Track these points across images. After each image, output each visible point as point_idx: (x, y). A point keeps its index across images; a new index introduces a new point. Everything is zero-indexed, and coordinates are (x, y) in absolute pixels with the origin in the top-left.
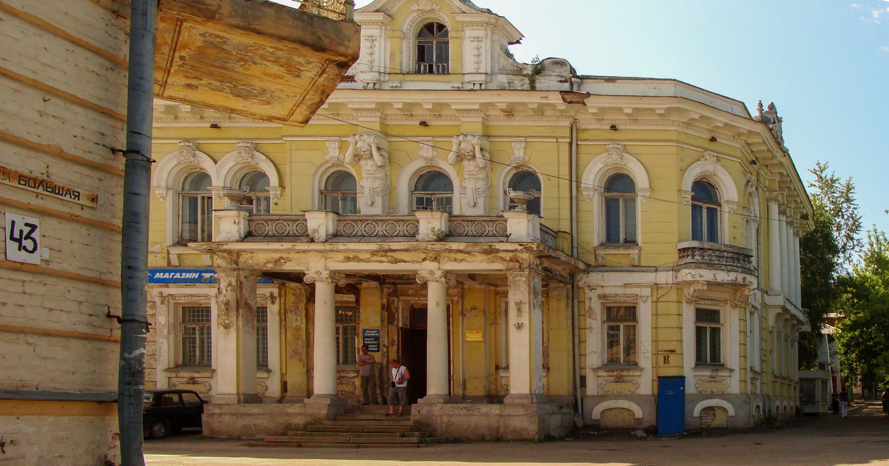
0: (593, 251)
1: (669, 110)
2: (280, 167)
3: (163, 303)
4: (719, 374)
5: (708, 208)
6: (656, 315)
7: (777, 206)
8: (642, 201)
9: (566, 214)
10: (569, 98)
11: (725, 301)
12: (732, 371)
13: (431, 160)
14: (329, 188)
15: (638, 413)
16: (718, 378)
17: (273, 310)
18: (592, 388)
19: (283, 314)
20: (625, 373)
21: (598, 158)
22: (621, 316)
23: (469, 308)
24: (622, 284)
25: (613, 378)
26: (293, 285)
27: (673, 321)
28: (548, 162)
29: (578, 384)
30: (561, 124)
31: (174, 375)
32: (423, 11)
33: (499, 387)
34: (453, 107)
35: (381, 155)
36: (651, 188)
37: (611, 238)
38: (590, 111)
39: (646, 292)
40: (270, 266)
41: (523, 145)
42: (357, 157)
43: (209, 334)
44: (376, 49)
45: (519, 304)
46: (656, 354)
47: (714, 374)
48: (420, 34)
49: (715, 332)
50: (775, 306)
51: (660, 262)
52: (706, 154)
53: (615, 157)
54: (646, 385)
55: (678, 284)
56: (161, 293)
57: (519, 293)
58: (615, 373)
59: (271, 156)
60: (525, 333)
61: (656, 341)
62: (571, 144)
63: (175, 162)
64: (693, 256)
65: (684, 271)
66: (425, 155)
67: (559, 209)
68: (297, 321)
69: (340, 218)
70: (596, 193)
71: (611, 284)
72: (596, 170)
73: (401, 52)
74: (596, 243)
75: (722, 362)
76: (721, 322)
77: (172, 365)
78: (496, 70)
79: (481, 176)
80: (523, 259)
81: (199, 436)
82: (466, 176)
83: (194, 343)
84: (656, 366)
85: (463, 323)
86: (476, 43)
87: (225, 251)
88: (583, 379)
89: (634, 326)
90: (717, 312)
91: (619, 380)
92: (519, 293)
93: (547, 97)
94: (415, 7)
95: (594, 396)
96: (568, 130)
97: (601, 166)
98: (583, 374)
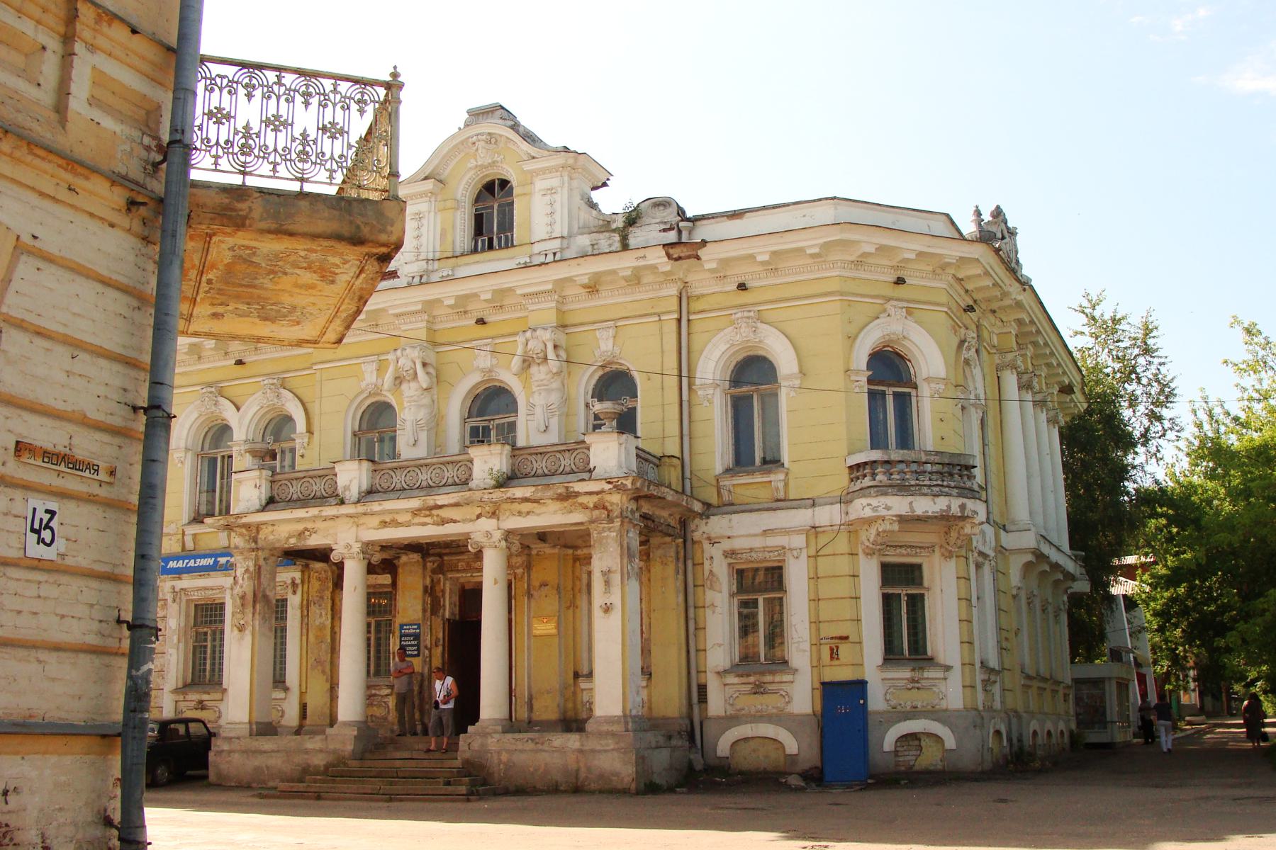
0: (714, 482)
1: (827, 246)
4: (926, 675)
5: (895, 395)
6: (815, 578)
7: (1015, 376)
8: (788, 394)
10: (675, 252)
11: (931, 548)
12: (948, 668)
13: (490, 371)
15: (791, 746)
16: (924, 683)
17: (294, 601)
18: (716, 704)
19: (306, 607)
20: (768, 678)
21: (718, 336)
22: (760, 583)
24: (759, 531)
26: (318, 566)
27: (843, 587)
30: (664, 292)
31: (181, 698)
32: (482, 167)
34: (519, 292)
36: (803, 373)
37: (742, 459)
38: (707, 266)
40: (293, 541)
42: (399, 380)
43: (222, 639)
45: (606, 574)
46: (816, 645)
47: (917, 675)
48: (477, 200)
49: (916, 602)
50: (1020, 551)
53: (745, 331)
54: (801, 696)
56: (173, 588)
58: (752, 679)
59: (299, 392)
61: (816, 623)
62: (679, 320)
63: (195, 415)
64: (874, 475)
67: (663, 421)
68: (321, 617)
72: (717, 354)
73: (454, 227)
74: (719, 469)
75: (929, 653)
76: (926, 583)
77: (180, 685)
80: (612, 504)
83: (205, 653)
84: (817, 666)
86: (548, 197)
88: (702, 689)
89: (781, 599)
90: (919, 567)
91: (759, 689)
92: (607, 557)
94: (472, 163)
95: (719, 718)
96: (675, 301)
97: (723, 347)
98: (703, 681)
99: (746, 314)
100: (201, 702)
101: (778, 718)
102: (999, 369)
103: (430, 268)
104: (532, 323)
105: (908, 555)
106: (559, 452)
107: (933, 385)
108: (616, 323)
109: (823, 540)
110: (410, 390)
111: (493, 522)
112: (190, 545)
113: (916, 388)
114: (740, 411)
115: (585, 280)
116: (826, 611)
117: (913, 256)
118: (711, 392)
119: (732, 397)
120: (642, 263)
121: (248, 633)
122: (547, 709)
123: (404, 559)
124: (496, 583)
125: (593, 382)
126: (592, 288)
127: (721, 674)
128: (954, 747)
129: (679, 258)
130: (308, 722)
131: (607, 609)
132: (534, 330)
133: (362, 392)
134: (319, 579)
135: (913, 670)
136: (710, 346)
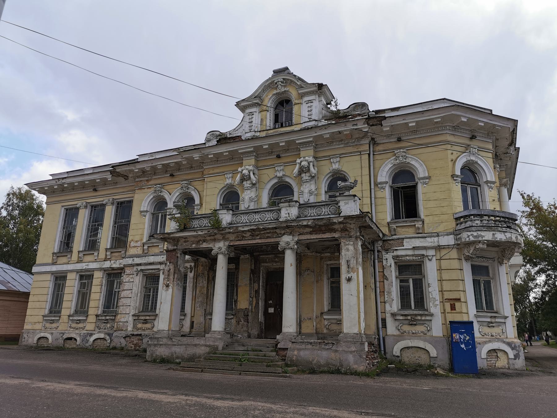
6: (440, 270)
10: (371, 122)
12: (506, 318)
15: (433, 353)
17: (191, 275)
18: (391, 328)
19: (196, 278)
22: (411, 270)
24: (411, 247)
26: (203, 259)
29: (380, 326)
42: (243, 179)
43: (157, 292)
46: (443, 301)
51: (441, 229)
54: (438, 328)
55: (458, 245)
62: (369, 154)
68: (203, 283)
69: (234, 213)
71: (409, 246)
72: (387, 168)
74: (389, 220)
83: (149, 298)
84: (444, 312)
87: (171, 238)
88: (384, 321)
90: (487, 268)
93: (356, 125)
96: (368, 145)
97: (390, 166)
100: (145, 320)
106: (322, 205)
111: (291, 237)
113: (480, 186)
121: (170, 290)
123: (242, 257)
124: (291, 265)
125: (328, 182)
128: (435, 356)
129: (373, 125)
131: (349, 280)
134: (202, 266)
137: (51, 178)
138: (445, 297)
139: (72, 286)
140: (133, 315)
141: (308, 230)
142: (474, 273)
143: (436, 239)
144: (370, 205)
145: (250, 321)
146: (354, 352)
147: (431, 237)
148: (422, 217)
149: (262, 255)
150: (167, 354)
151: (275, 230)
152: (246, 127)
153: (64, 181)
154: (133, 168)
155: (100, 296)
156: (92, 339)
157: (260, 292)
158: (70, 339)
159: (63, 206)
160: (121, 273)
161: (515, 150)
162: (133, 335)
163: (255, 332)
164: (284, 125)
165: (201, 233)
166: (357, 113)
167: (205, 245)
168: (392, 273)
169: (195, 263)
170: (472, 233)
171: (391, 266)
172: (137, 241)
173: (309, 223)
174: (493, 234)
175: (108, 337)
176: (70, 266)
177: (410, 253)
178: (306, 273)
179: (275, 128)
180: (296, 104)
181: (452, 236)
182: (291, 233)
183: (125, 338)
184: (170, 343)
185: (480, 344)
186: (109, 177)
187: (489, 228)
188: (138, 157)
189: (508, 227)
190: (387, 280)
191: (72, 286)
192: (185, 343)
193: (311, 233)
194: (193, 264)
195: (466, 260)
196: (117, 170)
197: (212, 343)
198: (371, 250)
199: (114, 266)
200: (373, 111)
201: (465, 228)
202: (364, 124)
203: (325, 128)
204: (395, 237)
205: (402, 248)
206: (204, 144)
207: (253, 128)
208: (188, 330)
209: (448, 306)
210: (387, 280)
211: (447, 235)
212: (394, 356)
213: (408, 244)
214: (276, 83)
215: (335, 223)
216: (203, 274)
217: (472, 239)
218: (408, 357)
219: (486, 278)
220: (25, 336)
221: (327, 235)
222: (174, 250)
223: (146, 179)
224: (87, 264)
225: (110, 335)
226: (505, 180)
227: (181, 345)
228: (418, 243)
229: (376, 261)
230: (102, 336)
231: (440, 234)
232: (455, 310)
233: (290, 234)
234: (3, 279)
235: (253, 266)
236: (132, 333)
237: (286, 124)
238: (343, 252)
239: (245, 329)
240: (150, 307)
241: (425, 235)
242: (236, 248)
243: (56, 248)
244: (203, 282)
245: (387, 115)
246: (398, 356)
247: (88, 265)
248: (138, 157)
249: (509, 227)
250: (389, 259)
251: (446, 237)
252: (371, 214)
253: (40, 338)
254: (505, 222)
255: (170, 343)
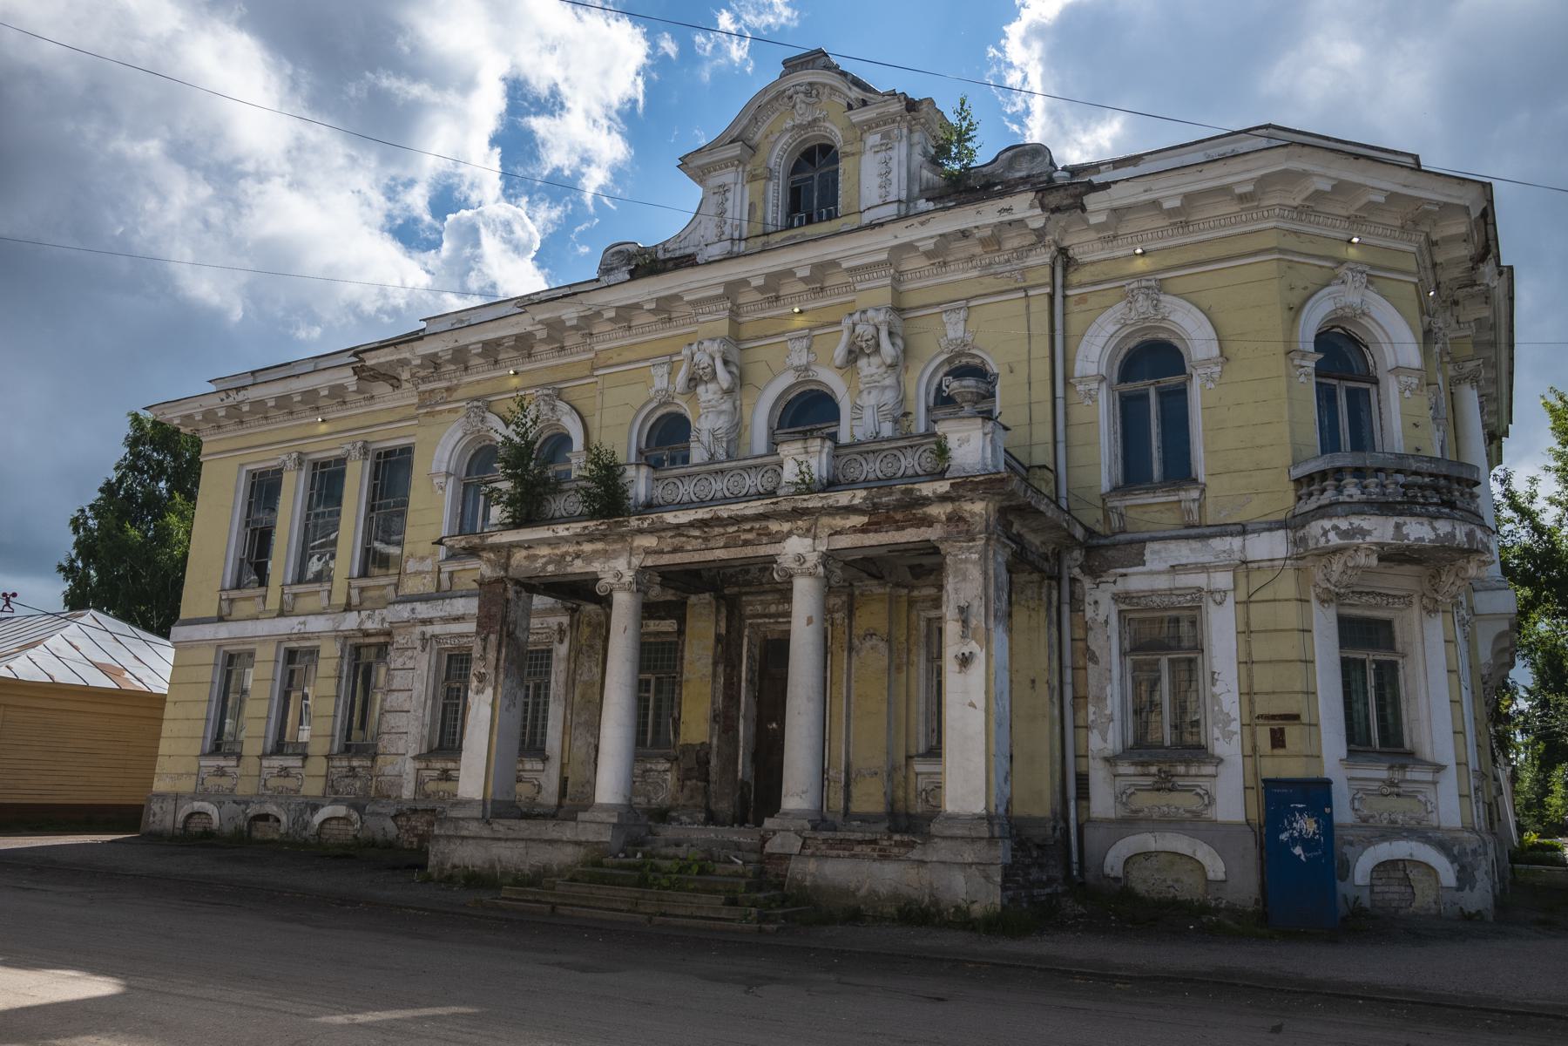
0: (1100, 504)
1: (1263, 182)
2: (588, 419)
3: (424, 650)
4: (1408, 776)
5: (1349, 392)
6: (1246, 632)
7: (1475, 393)
8: (1203, 387)
9: (1043, 433)
10: (1053, 199)
11: (1407, 600)
12: (1439, 768)
13: (807, 369)
14: (653, 444)
15: (1216, 868)
16: (1405, 787)
17: (562, 650)
18: (1102, 802)
20: (1181, 769)
21: (1106, 315)
22: (1166, 638)
23: (862, 633)
24: (1164, 566)
25: (1148, 781)
27: (1287, 647)
28: (1006, 336)
30: (1031, 261)
31: (423, 765)
32: (800, 127)
33: (912, 796)
34: (845, 265)
35: (730, 372)
36: (1225, 357)
37: (1134, 475)
38: (1093, 220)
39: (1223, 580)
40: (551, 568)
41: (962, 314)
42: (694, 381)
44: (729, 205)
45: (963, 611)
47: (1397, 775)
48: (796, 169)
49: (1388, 674)
50: (1495, 616)
52: (1342, 271)
53: (1142, 304)
54: (1230, 797)
56: (423, 634)
57: (968, 581)
58: (1154, 769)
59: (577, 404)
60: (978, 669)
61: (1248, 694)
62: (1052, 297)
63: (460, 434)
64: (1339, 490)
65: (1316, 528)
66: (796, 362)
67: (1030, 424)
70: (1104, 386)
72: (1101, 341)
73: (765, 201)
74: (1105, 486)
75: (1407, 745)
76: (1399, 646)
77: (424, 750)
78: (916, 189)
79: (887, 382)
80: (973, 514)
81: (416, 876)
82: (862, 387)
84: (1252, 754)
85: (849, 664)
86: (883, 154)
88: (1083, 781)
89: (1191, 661)
90: (1388, 624)
91: (1165, 784)
92: (968, 581)
93: (1009, 210)
94: (789, 124)
95: (1110, 821)
96: (1047, 271)
98: (1083, 769)
99: (1144, 283)
100: (445, 771)
101: (1196, 824)
102: (1455, 382)
103: (736, 249)
104: (860, 305)
105: (1370, 607)
107: (1403, 379)
108: (965, 304)
109: (1257, 580)
110: (707, 393)
111: (809, 541)
112: (446, 584)
113: (1376, 382)
114: (1130, 412)
115: (929, 245)
116: (1264, 679)
117: (1382, 199)
118: (1095, 385)
119: (1122, 395)
120: (1007, 217)
122: (870, 798)
123: (693, 599)
126: (939, 254)
127: (1111, 761)
128: (1221, 876)
130: (567, 801)
131: (965, 661)
132: (864, 312)
133: (651, 400)
134: (589, 624)
135: (1391, 768)
136: (1095, 326)
137: (213, 388)
138: (1259, 711)
139: (260, 680)
140: (414, 758)
141: (858, 520)
142: (1344, 642)
143: (1237, 542)
144: (1050, 447)
145: (713, 777)
146: (970, 865)
147: (1222, 535)
148: (1202, 478)
149: (746, 594)
150: (479, 863)
151: (764, 524)
152: (711, 232)
153: (241, 396)
154: (408, 355)
155: (337, 706)
156: (318, 818)
157: (743, 698)
158: (265, 817)
159: (242, 465)
160: (386, 645)
161: (1501, 274)
162: (415, 811)
163: (724, 806)
164: (815, 217)
165: (566, 533)
166: (1018, 175)
167: (578, 567)
168: (1108, 644)
169: (572, 617)
170: (1335, 521)
171: (1106, 622)
172: (423, 559)
173: (856, 501)
174: (1398, 527)
175: (355, 816)
176: (261, 630)
177: (1162, 583)
178: (868, 644)
179: (790, 227)
180: (847, 155)
181: (1281, 533)
182: (808, 530)
183: (394, 818)
184: (486, 833)
185: (1351, 844)
186: (348, 378)
187: (1384, 508)
188: (424, 325)
189: (1444, 503)
190: (1096, 662)
191: (260, 680)
192: (526, 834)
193: (864, 530)
194: (565, 620)
195: (1323, 601)
196: (368, 363)
197: (591, 838)
198: (1050, 578)
199: (370, 626)
200: (1064, 169)
201: (1319, 507)
202: (1032, 206)
203: (922, 224)
204: (1121, 537)
205: (1140, 569)
206: (597, 280)
207: (727, 230)
208: (553, 800)
209: (1264, 736)
210: (1096, 662)
211: (1270, 530)
212: (1107, 877)
213: (1159, 557)
214: (791, 97)
215: (926, 498)
216: (591, 647)
217: (1334, 540)
218: (1145, 881)
219: (1383, 656)
220: (156, 807)
221: (910, 535)
222: (499, 580)
223: (444, 384)
224: (302, 619)
225: (358, 807)
226: (1470, 365)
227: (514, 840)
228: (1184, 552)
229: (1066, 609)
230: (341, 810)
231: (1249, 528)
232: (1283, 746)
233: (807, 532)
234: (110, 661)
235: (723, 624)
236: (412, 805)
237: (820, 215)
238: (950, 584)
239: (699, 799)
240: (649, 736)
241: (1207, 531)
242: (668, 576)
243: (228, 577)
244: (590, 670)
245: (1096, 179)
246: (1117, 879)
247: (304, 623)
248: (424, 325)
249: (1451, 505)
250: (1101, 602)
251: (1265, 535)
252: (1055, 472)
253: (190, 816)
254: (1437, 490)
255: (486, 833)
